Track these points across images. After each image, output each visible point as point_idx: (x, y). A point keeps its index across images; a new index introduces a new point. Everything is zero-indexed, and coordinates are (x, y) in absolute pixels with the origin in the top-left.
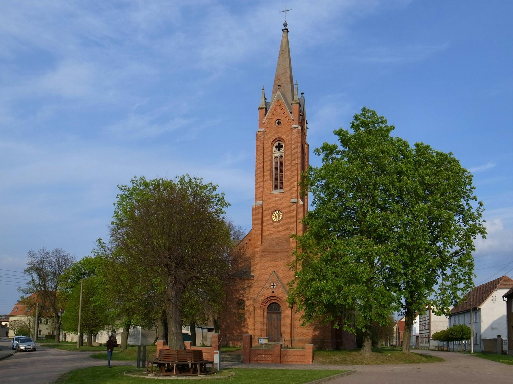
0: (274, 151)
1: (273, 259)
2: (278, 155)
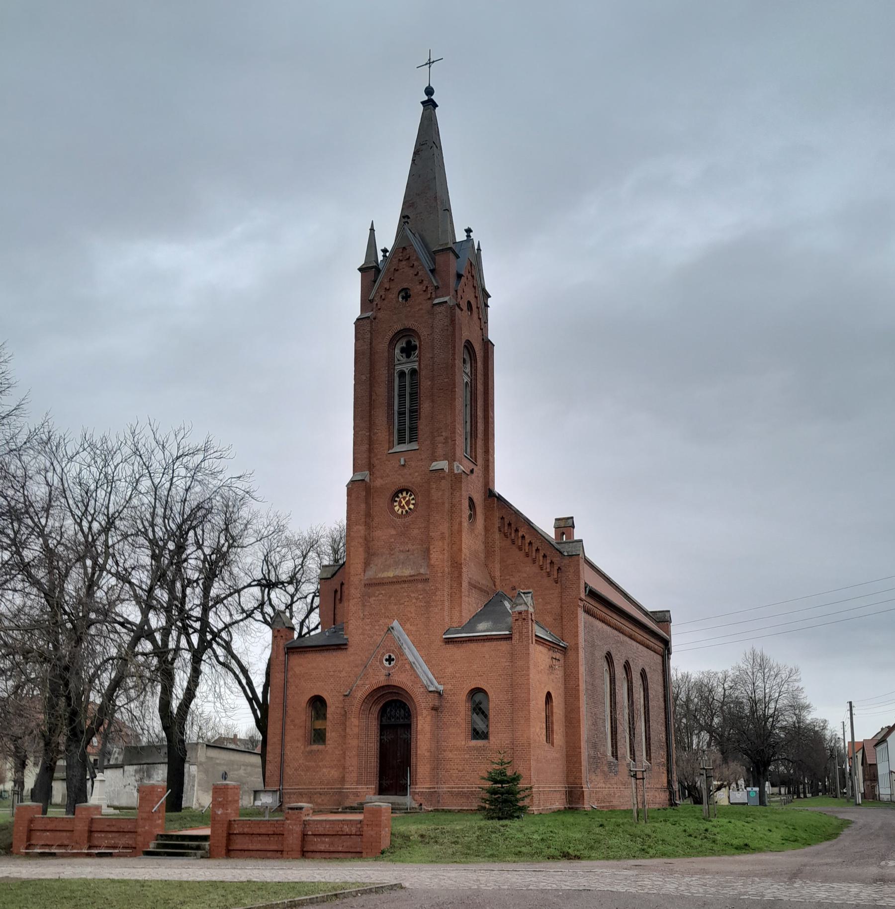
0: (396, 359)
1: (392, 599)
2: (406, 368)
